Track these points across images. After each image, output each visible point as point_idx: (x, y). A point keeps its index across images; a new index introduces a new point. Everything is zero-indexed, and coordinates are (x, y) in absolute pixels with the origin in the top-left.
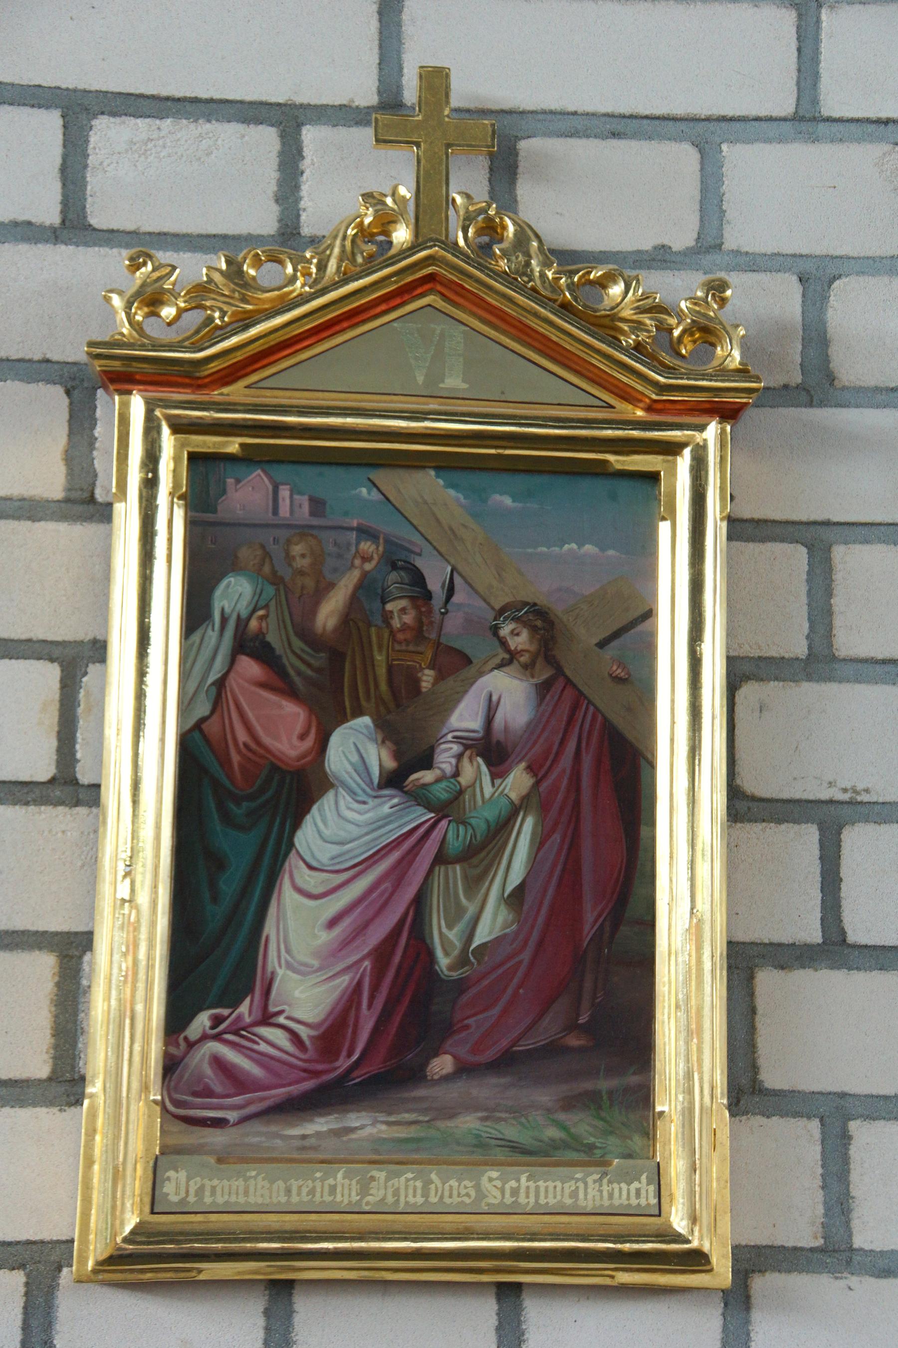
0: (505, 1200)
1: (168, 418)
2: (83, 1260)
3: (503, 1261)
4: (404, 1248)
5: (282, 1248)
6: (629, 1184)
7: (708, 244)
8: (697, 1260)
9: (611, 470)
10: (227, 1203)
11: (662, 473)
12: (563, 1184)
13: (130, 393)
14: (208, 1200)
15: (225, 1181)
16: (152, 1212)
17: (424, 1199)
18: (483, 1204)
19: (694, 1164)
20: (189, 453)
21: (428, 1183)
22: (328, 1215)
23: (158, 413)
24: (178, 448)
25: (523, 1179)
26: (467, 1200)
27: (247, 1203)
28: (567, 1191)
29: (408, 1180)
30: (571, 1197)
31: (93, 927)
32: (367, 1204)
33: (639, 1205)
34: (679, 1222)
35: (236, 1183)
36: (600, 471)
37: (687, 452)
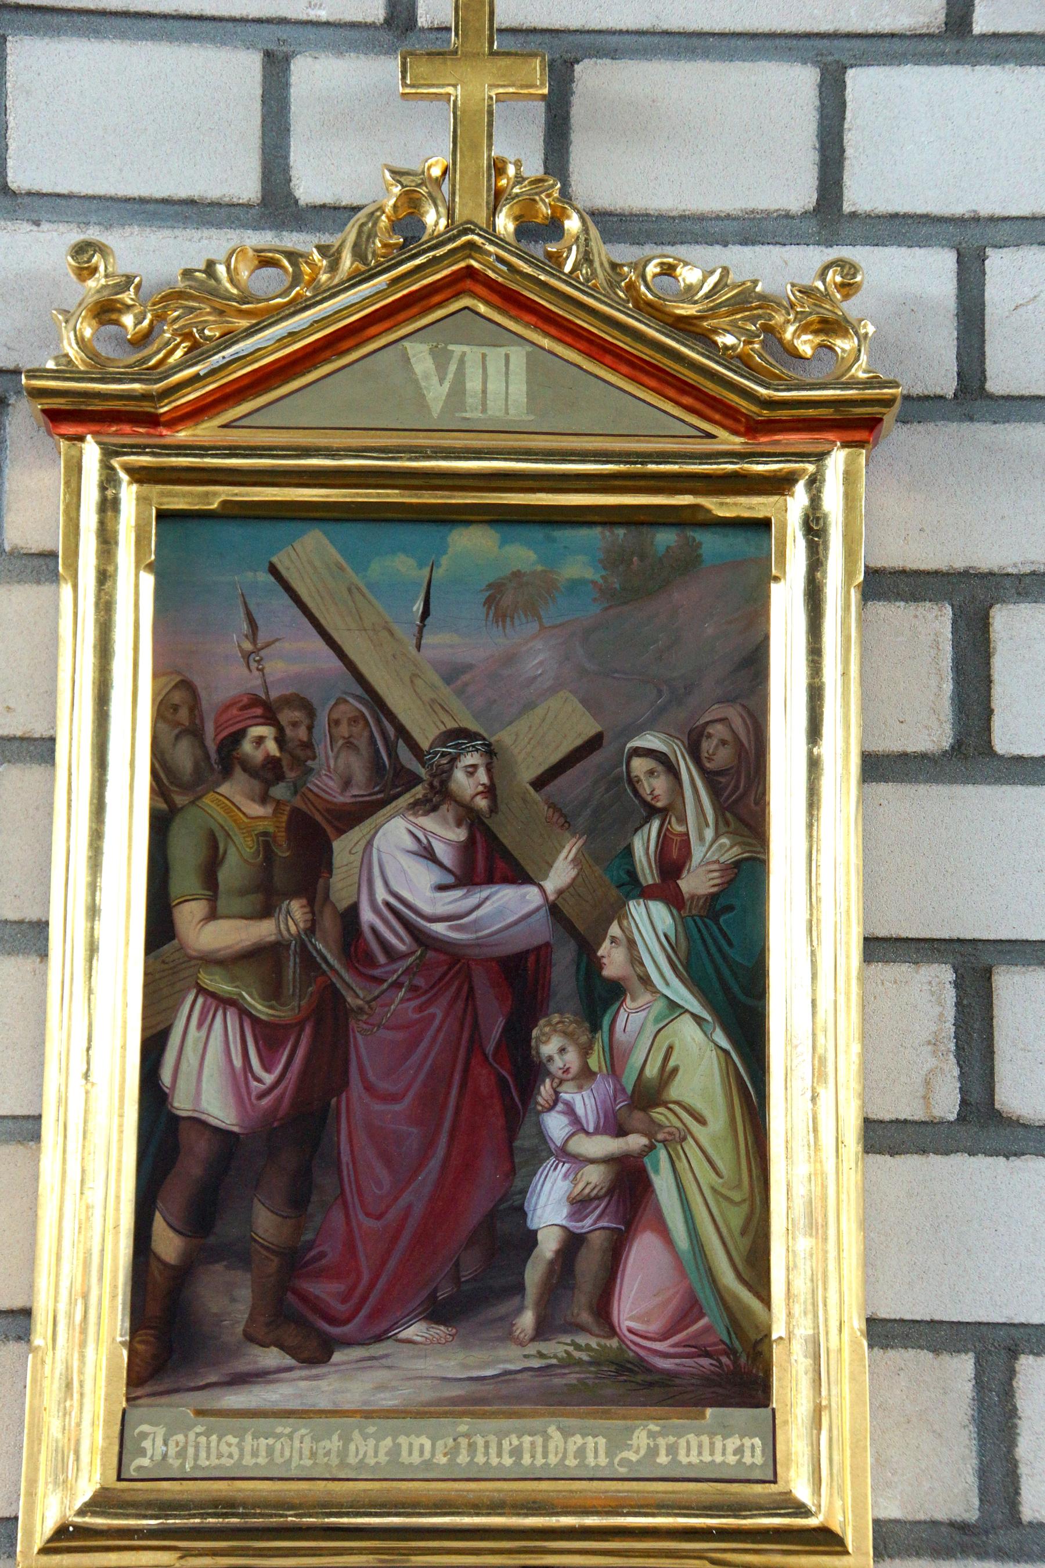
1: (130, 470)
2: (29, 1534)
3: (268, 1540)
4: (442, 1524)
7: (829, 215)
13: (81, 439)
16: (119, 1479)
17: (311, 1462)
20: (158, 511)
21: (547, 1438)
22: (607, 1483)
23: (115, 463)
24: (142, 500)
28: (730, 1450)
29: (198, 1435)
33: (546, 1464)
34: (803, 1493)
37: (800, 488)
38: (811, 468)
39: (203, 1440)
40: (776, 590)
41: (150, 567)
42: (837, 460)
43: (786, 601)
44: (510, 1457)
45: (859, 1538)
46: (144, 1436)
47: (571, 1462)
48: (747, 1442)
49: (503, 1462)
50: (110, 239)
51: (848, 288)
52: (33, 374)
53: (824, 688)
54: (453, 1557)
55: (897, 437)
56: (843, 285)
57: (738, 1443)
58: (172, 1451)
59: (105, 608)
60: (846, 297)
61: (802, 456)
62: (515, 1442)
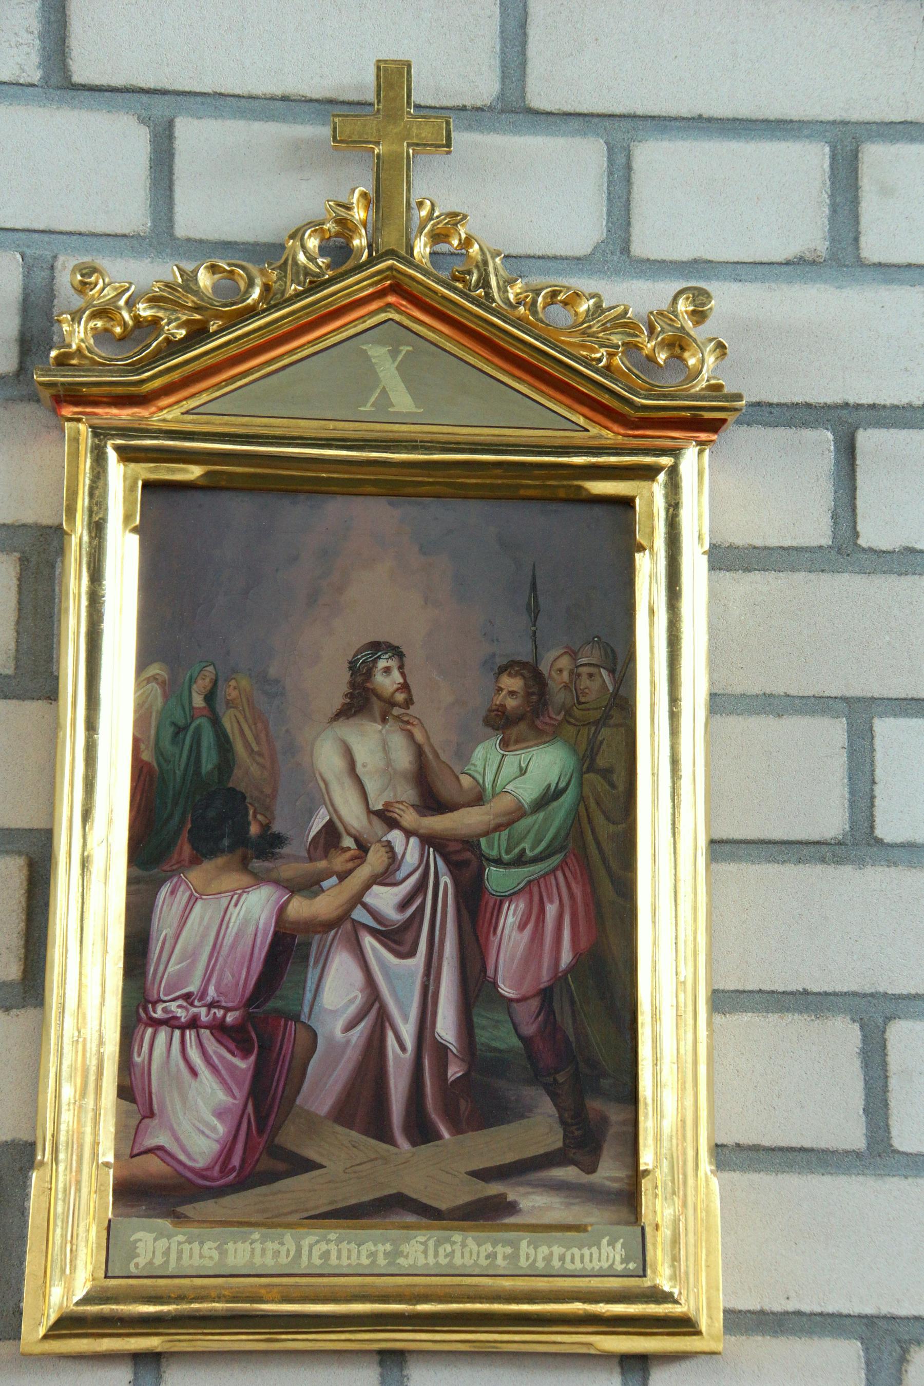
0: (255, 1261)
1: (118, 448)
5: (228, 1310)
8: (684, 1325)
9: (584, 495)
10: (349, 1265)
11: (637, 501)
12: (359, 1245)
15: (380, 1245)
16: (106, 1277)
18: (132, 1266)
19: (696, 1233)
25: (524, 1244)
27: (264, 1265)
28: (483, 1255)
29: (180, 1243)
33: (427, 1264)
34: (663, 1280)
35: (348, 1246)
37: (662, 477)
38: (666, 461)
39: (186, 1247)
40: (642, 561)
41: (135, 530)
42: (691, 461)
43: (648, 569)
50: (103, 262)
51: (699, 316)
53: (681, 640)
54: (339, 1348)
55: (735, 436)
56: (694, 312)
60: (697, 323)
61: (662, 452)
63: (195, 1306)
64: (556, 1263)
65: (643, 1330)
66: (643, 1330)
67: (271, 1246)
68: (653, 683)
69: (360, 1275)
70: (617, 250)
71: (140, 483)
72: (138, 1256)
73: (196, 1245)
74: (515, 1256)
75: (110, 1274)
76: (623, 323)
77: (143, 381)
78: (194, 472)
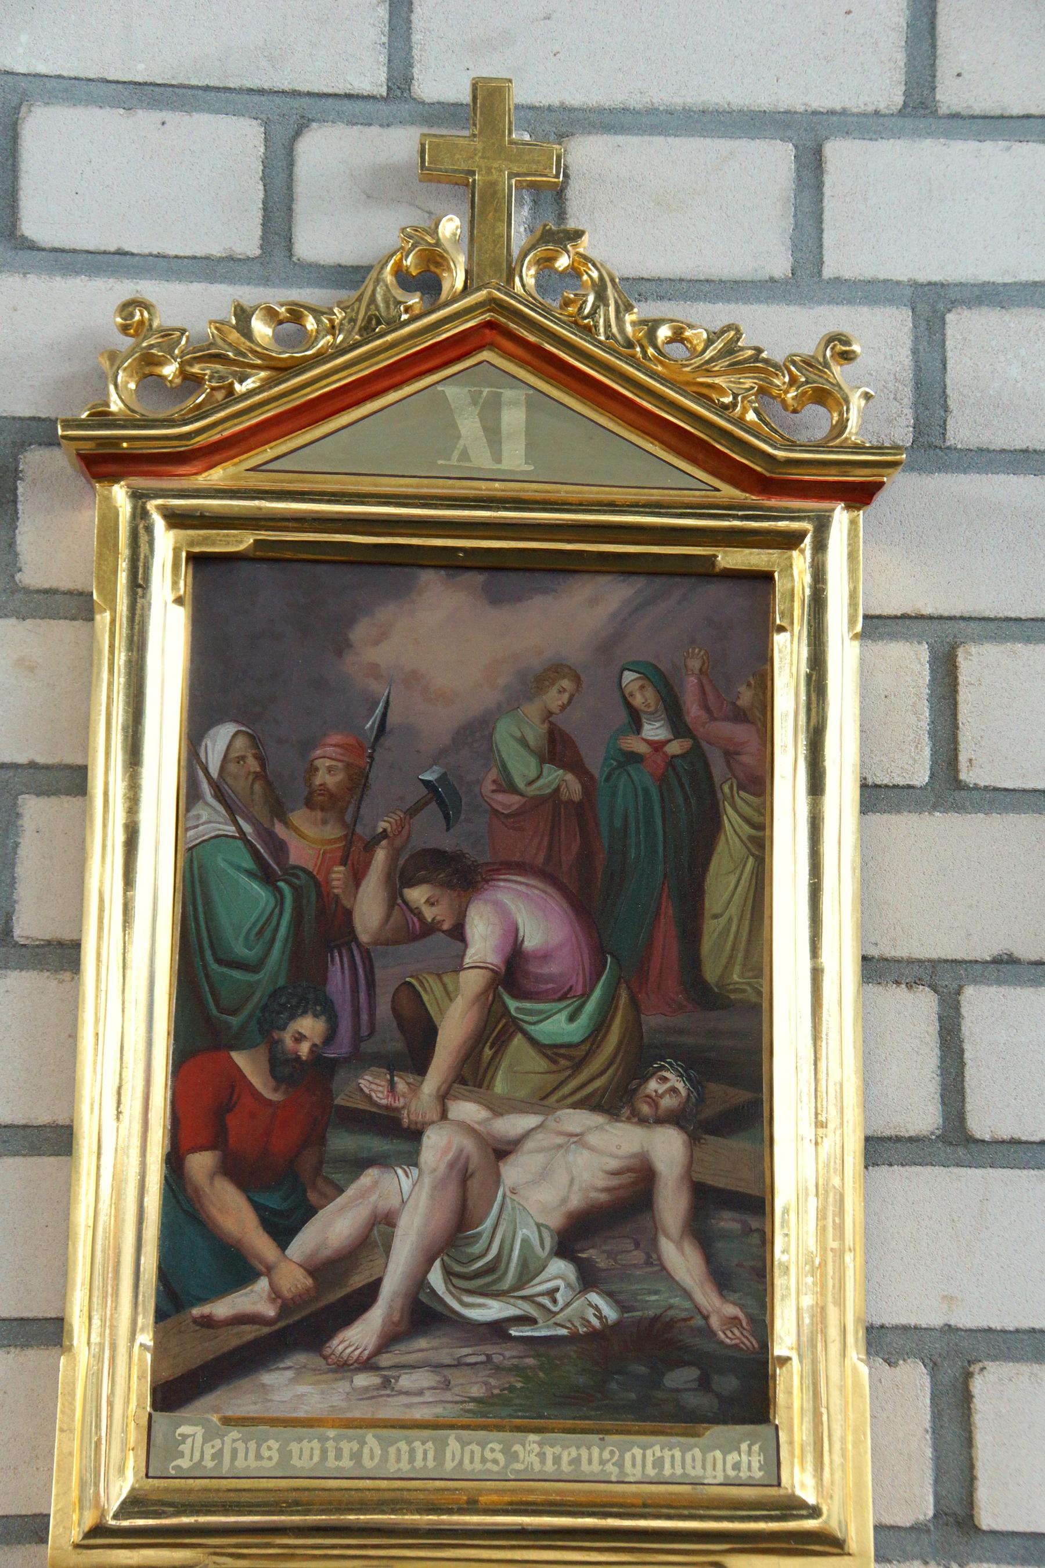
1: (158, 508)
6: (725, 1454)
11: (776, 575)
14: (667, 1471)
16: (147, 1476)
26: (495, 1468)
29: (234, 1441)
30: (733, 1469)
31: (64, 1310)
32: (514, 1471)
35: (310, 1445)
36: (705, 572)
40: (780, 641)
43: (788, 653)
44: (351, 1460)
45: (861, 1537)
46: (185, 1437)
47: (565, 1467)
48: (667, 1454)
49: (742, 1474)
52: (68, 424)
55: (900, 489)
57: (574, 1453)
58: (209, 1452)
59: (137, 644)
62: (658, 1454)
63: (455, 1518)
64: (565, 1467)
65: (553, 1543)
66: (553, 1543)
67: (346, 1447)
68: (816, 786)
69: (441, 1479)
70: (806, 277)
71: (184, 554)
72: (182, 1455)
73: (252, 1445)
74: (440, 1458)
75: (775, 1483)
76: (757, 364)
77: (188, 436)
78: (243, 541)
